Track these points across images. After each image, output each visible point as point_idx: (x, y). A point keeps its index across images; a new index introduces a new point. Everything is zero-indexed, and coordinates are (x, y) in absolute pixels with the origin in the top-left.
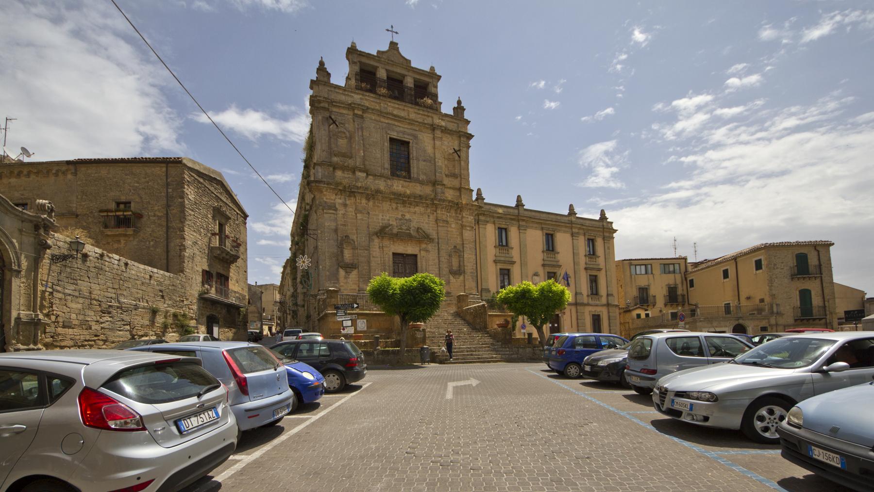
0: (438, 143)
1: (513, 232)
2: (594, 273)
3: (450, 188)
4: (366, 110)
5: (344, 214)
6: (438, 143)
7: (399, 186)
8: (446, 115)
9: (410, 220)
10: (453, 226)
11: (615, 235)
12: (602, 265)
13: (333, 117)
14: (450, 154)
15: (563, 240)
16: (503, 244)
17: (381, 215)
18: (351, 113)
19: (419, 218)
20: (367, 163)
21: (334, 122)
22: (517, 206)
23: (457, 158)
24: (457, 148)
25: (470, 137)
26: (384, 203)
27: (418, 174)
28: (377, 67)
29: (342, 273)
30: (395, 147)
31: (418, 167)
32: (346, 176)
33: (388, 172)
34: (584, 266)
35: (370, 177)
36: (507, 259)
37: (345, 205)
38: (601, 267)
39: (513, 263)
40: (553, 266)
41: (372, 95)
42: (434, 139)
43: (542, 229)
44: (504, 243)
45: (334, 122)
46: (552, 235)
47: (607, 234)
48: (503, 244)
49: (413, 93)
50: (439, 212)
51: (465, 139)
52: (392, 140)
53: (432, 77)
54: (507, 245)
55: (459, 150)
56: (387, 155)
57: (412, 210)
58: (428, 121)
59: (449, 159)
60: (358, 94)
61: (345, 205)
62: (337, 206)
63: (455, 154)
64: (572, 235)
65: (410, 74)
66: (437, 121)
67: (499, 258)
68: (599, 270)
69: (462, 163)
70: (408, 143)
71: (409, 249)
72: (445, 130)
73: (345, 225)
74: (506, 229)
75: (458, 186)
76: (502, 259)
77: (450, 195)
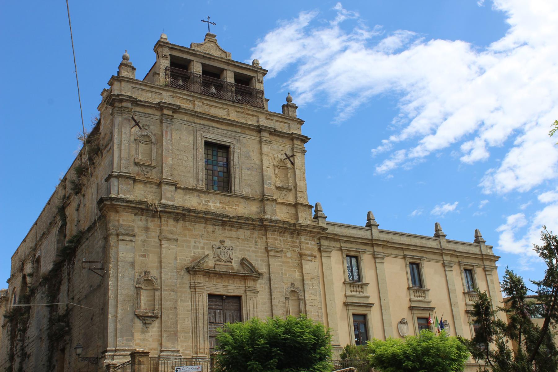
0: (266, 149)
1: (366, 261)
2: (425, 314)
3: (283, 204)
4: (176, 110)
5: (144, 241)
6: (266, 149)
7: (215, 204)
8: (275, 115)
9: (231, 249)
10: (289, 255)
11: (497, 264)
12: (373, 299)
13: (136, 118)
14: (281, 161)
15: (431, 272)
16: (356, 281)
17: (193, 240)
18: (158, 113)
19: (243, 247)
20: (175, 173)
21: (137, 124)
22: (369, 225)
23: (289, 165)
24: (289, 154)
25: (304, 139)
26: (197, 225)
27: (241, 186)
28: (191, 61)
29: (138, 324)
30: (210, 152)
31: (243, 179)
32: (349, 109)
33: (202, 185)
34: (343, 299)
35: (179, 191)
36: (361, 301)
37: (147, 229)
38: (370, 301)
39: (370, 306)
40: (424, 309)
41: (185, 92)
42: (260, 142)
43: (404, 257)
44: (356, 278)
45: (137, 124)
46: (417, 265)
47: (487, 263)
48: (356, 281)
49: (234, 89)
50: (269, 236)
51: (299, 143)
52: (208, 144)
53: (256, 72)
54: (359, 280)
55: (292, 156)
56: (201, 164)
57: (233, 233)
58: (252, 121)
59: (279, 167)
60: (167, 91)
61: (147, 229)
62: (136, 230)
63: (287, 161)
64: (444, 265)
65: (230, 68)
66: (263, 121)
67: (349, 300)
68: (370, 306)
69: (297, 171)
70: (229, 147)
71: (231, 288)
72: (274, 133)
73: (144, 256)
74: (356, 257)
75: (292, 201)
76: (356, 300)
77: (282, 214)
